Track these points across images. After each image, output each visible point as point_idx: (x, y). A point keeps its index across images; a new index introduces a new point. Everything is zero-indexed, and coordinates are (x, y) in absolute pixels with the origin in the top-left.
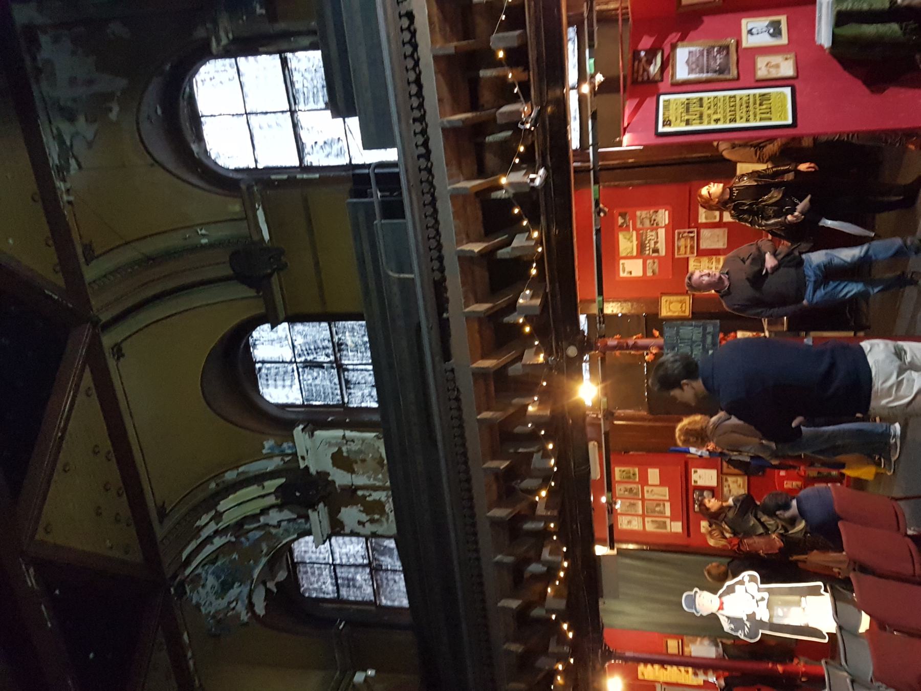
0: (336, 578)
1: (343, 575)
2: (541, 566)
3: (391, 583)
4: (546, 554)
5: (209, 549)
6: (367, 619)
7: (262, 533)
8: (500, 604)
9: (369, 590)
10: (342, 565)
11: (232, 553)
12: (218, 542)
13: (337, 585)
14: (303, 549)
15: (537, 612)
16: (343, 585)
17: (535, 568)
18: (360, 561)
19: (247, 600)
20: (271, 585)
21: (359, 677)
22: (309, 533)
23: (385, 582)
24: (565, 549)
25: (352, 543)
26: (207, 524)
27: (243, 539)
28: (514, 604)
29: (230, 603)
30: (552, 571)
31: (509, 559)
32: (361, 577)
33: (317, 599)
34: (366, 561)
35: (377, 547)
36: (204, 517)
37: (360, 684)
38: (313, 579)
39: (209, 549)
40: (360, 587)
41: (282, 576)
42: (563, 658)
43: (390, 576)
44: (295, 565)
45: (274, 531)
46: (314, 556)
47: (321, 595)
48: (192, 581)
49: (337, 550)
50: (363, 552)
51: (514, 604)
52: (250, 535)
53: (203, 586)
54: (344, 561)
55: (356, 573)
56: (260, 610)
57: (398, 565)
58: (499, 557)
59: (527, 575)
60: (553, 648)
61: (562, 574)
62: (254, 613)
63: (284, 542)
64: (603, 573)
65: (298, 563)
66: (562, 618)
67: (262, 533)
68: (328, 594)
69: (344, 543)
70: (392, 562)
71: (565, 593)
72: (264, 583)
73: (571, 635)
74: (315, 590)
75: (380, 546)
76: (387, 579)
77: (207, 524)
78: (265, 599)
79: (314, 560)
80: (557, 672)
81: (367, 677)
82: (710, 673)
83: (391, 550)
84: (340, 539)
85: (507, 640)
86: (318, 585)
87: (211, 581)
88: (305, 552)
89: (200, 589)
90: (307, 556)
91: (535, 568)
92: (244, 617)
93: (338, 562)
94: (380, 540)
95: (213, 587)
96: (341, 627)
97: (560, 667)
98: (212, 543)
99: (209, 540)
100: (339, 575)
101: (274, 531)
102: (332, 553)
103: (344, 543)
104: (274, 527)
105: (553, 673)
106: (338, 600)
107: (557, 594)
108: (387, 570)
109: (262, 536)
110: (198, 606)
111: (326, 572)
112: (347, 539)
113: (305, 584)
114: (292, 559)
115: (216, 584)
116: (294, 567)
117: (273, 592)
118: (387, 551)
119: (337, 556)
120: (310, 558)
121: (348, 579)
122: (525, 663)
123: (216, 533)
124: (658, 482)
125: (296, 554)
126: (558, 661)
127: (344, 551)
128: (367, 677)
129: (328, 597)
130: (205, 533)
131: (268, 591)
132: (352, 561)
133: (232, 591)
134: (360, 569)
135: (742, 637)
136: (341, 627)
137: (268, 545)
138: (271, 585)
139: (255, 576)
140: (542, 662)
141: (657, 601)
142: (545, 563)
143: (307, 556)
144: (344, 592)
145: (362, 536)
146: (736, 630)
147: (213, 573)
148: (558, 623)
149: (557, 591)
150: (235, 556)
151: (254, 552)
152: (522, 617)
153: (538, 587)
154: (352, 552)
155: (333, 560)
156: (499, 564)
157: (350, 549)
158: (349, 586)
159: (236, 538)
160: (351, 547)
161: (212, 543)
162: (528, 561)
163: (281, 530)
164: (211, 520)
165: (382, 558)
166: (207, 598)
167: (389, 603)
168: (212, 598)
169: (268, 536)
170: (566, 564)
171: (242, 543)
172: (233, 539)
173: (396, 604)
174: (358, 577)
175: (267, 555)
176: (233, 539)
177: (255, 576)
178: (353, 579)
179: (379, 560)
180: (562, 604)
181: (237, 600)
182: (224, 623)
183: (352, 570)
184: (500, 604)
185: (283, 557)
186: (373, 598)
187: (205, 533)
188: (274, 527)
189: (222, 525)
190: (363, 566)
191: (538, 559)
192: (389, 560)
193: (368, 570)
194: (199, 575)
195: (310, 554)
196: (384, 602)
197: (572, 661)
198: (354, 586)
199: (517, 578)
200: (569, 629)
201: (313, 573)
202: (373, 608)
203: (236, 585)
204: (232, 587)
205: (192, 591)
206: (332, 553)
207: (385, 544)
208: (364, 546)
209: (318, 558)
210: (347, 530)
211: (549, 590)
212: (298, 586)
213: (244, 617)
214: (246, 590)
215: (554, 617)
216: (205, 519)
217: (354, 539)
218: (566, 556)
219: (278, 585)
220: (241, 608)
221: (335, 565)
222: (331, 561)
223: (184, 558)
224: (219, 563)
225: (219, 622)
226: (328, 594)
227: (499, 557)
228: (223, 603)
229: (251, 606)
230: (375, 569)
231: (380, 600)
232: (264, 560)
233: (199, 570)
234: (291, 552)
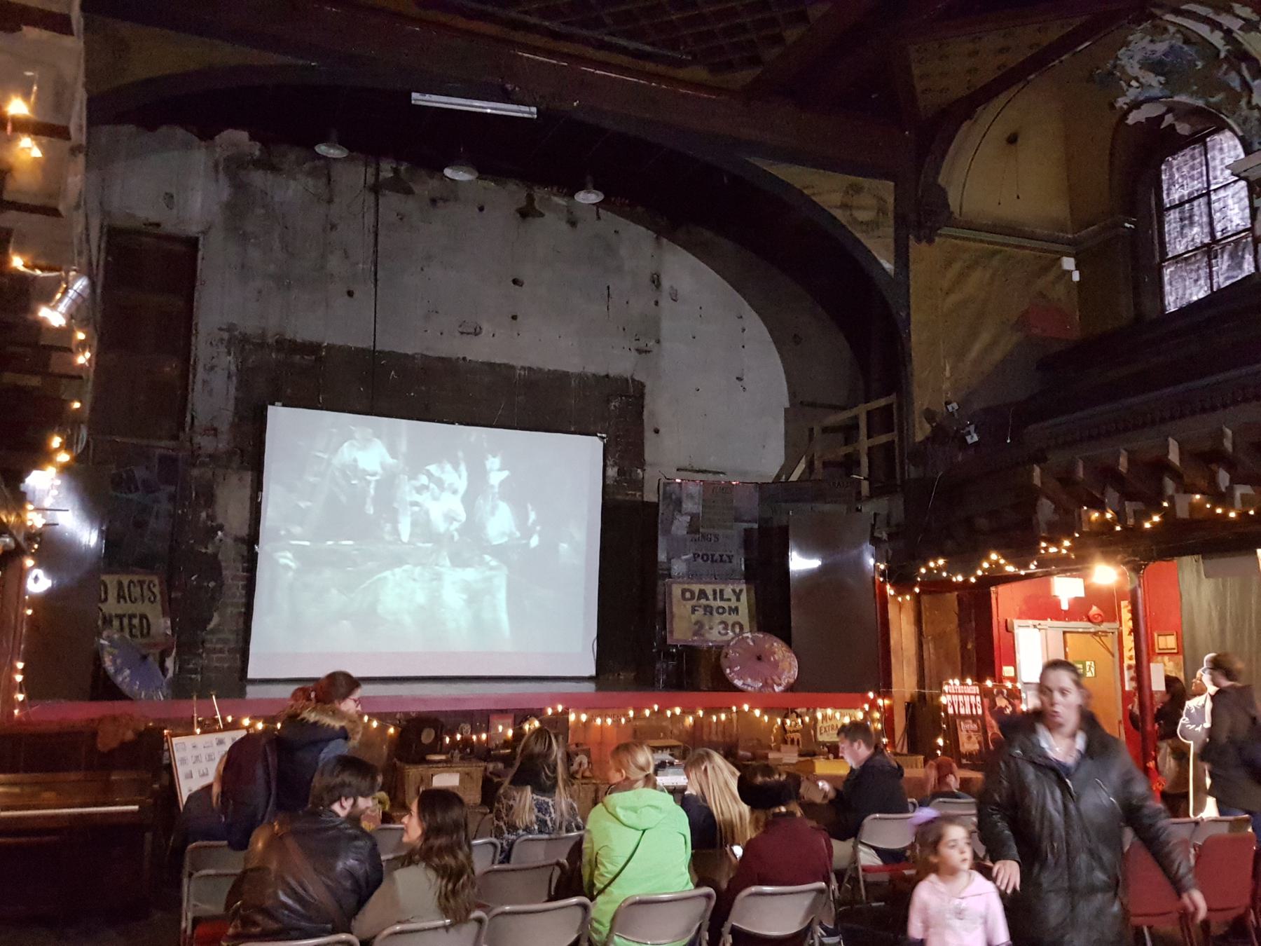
0: (1190, 201)
1: (1196, 209)
2: (1227, 484)
3: (1194, 276)
4: (1240, 490)
5: (1204, 30)
6: (1143, 257)
7: (1239, 89)
8: (1171, 440)
9: (1180, 249)
10: (1209, 204)
11: (1203, 59)
12: (1217, 38)
13: (1181, 204)
14: (1225, 145)
15: (1170, 485)
16: (1182, 212)
17: (1224, 478)
18: (1219, 227)
19: (1142, 93)
20: (1169, 119)
21: (1068, 263)
22: (1248, 151)
23: (1195, 267)
24: (1252, 512)
25: (1243, 210)
26: (1238, 16)
27: (1225, 66)
28: (1174, 457)
29: (1137, 80)
30: (1223, 498)
31: (1228, 445)
32: (1198, 234)
33: (1160, 181)
34: (1219, 235)
35: (1240, 248)
36: (1248, 10)
37: (1061, 266)
38: (1185, 169)
39: (1204, 30)
40: (1182, 235)
41: (1183, 129)
42: (1120, 516)
43: (1203, 272)
44: (1202, 141)
45: (1243, 103)
46: (1217, 162)
47: (1165, 187)
48: (1155, 27)
49: (1230, 191)
50: (1231, 228)
51: (1174, 457)
52: (1233, 74)
53: (1152, 41)
54: (1215, 206)
55: (1201, 226)
56: (1132, 118)
57: (1222, 281)
58: (1229, 432)
59: (1214, 467)
60: (1129, 507)
61: (1219, 511)
62: (1130, 110)
63: (1229, 121)
64: (1223, 560)
65: (1205, 144)
66: (1168, 515)
67: (1239, 89)
68: (1168, 194)
69: (1241, 199)
70: (1224, 274)
71: (1197, 516)
72: (1168, 112)
73: (1147, 525)
74: (1172, 176)
75: (1244, 250)
76: (1199, 268)
77: (1238, 16)
78: (1147, 119)
79: (1211, 164)
80: (1103, 512)
81: (1070, 272)
82: (1134, 684)
83: (1240, 266)
84: (1244, 193)
85: (1130, 452)
86: (1179, 180)
87: (1161, 47)
88: (1221, 149)
89: (1149, 38)
90: (1216, 153)
91: (1224, 478)
92: (1121, 102)
93: (1214, 197)
94: (1251, 247)
95: (1154, 52)
96: (1127, 225)
97: (1109, 516)
98: (1212, 31)
99: (1216, 26)
100: (1196, 203)
101: (1243, 103)
102: (1225, 186)
103: (1241, 199)
104: (1249, 102)
105: (1101, 508)
106: (1162, 210)
107: (1193, 507)
108: (1210, 266)
109: (1232, 89)
110: (1126, 44)
111: (1197, 185)
112: (1246, 202)
113: (1177, 160)
114: (1209, 135)
115: (1158, 54)
116: (1199, 139)
117: (1160, 124)
118: (1237, 262)
119: (1222, 193)
120: (1214, 159)
121: (1191, 217)
122: (1109, 475)
123: (1228, 33)
124: (905, 750)
125: (1216, 137)
126: (1116, 513)
127: (1230, 202)
128: (1070, 272)
129: (1165, 196)
130: (1226, 20)
131: (1161, 118)
132: (1217, 216)
133: (1152, 75)
134: (1206, 230)
135: (1181, 721)
136: (1127, 225)
137: (1221, 101)
138: (1169, 119)
139: (1176, 98)
140: (1112, 496)
141: (1222, 618)
142: (1230, 489)
143: (1216, 153)
144: (1173, 215)
145: (1252, 223)
146: (1188, 715)
147: (1172, 47)
148: (1159, 509)
149: (1200, 506)
150: (1200, 64)
151: (1209, 85)
152: (1161, 467)
153: (1203, 483)
154: (1229, 213)
155: (1215, 190)
156: (1222, 435)
157: (1233, 210)
158: (1182, 220)
159: (1226, 57)
160: (1237, 210)
161: (1212, 31)
162: (1231, 465)
163: (1245, 112)
164: (1244, 19)
165: (1226, 257)
166: (1137, 50)
167: (1166, 278)
168: (1138, 57)
169: (1234, 98)
170: (1232, 515)
171: (1220, 67)
172: (1222, 55)
173: (1167, 288)
174: (1196, 230)
175: (1207, 103)
176: (1222, 55)
177: (1176, 98)
178: (1192, 224)
179: (1222, 253)
180: (1182, 512)
181: (1142, 85)
182: (1111, 81)
183: (1205, 219)
184: (1171, 440)
185: (1207, 125)
186: (1170, 255)
187: (1226, 20)
188: (1249, 102)
189: (1239, 35)
190: (1212, 233)
191: (1234, 481)
192: (1225, 267)
193: (1207, 240)
194: (1166, 30)
195: (1219, 157)
196: (1167, 273)
197: (1118, 528)
198: (1182, 228)
199: (1207, 457)
200: (1153, 524)
201: (1193, 168)
202: (1158, 259)
203: (1162, 79)
204: (1157, 74)
205: (1145, 31)
206: (1225, 186)
207: (1247, 256)
208: (1241, 228)
209: (1215, 168)
210: (1258, 203)
211: (1198, 497)
212: (1173, 153)
213: (1121, 102)
214: (1156, 92)
215: (1165, 504)
216: (1246, 12)
217: (1247, 211)
218: (1243, 515)
219: (1172, 127)
220: (1132, 94)
221: (1208, 194)
222: (1212, 187)
223: (1184, 7)
224: (1186, 48)
225: (1111, 74)
226: (1168, 194)
227: (1229, 432)
228: (1133, 68)
229: (1136, 105)
230: (1209, 250)
231: (1168, 267)
232: (1200, 103)
233: (1172, 29)
234: (1219, 130)
